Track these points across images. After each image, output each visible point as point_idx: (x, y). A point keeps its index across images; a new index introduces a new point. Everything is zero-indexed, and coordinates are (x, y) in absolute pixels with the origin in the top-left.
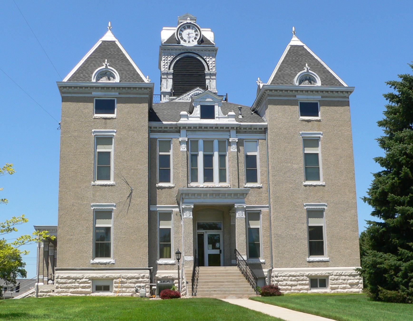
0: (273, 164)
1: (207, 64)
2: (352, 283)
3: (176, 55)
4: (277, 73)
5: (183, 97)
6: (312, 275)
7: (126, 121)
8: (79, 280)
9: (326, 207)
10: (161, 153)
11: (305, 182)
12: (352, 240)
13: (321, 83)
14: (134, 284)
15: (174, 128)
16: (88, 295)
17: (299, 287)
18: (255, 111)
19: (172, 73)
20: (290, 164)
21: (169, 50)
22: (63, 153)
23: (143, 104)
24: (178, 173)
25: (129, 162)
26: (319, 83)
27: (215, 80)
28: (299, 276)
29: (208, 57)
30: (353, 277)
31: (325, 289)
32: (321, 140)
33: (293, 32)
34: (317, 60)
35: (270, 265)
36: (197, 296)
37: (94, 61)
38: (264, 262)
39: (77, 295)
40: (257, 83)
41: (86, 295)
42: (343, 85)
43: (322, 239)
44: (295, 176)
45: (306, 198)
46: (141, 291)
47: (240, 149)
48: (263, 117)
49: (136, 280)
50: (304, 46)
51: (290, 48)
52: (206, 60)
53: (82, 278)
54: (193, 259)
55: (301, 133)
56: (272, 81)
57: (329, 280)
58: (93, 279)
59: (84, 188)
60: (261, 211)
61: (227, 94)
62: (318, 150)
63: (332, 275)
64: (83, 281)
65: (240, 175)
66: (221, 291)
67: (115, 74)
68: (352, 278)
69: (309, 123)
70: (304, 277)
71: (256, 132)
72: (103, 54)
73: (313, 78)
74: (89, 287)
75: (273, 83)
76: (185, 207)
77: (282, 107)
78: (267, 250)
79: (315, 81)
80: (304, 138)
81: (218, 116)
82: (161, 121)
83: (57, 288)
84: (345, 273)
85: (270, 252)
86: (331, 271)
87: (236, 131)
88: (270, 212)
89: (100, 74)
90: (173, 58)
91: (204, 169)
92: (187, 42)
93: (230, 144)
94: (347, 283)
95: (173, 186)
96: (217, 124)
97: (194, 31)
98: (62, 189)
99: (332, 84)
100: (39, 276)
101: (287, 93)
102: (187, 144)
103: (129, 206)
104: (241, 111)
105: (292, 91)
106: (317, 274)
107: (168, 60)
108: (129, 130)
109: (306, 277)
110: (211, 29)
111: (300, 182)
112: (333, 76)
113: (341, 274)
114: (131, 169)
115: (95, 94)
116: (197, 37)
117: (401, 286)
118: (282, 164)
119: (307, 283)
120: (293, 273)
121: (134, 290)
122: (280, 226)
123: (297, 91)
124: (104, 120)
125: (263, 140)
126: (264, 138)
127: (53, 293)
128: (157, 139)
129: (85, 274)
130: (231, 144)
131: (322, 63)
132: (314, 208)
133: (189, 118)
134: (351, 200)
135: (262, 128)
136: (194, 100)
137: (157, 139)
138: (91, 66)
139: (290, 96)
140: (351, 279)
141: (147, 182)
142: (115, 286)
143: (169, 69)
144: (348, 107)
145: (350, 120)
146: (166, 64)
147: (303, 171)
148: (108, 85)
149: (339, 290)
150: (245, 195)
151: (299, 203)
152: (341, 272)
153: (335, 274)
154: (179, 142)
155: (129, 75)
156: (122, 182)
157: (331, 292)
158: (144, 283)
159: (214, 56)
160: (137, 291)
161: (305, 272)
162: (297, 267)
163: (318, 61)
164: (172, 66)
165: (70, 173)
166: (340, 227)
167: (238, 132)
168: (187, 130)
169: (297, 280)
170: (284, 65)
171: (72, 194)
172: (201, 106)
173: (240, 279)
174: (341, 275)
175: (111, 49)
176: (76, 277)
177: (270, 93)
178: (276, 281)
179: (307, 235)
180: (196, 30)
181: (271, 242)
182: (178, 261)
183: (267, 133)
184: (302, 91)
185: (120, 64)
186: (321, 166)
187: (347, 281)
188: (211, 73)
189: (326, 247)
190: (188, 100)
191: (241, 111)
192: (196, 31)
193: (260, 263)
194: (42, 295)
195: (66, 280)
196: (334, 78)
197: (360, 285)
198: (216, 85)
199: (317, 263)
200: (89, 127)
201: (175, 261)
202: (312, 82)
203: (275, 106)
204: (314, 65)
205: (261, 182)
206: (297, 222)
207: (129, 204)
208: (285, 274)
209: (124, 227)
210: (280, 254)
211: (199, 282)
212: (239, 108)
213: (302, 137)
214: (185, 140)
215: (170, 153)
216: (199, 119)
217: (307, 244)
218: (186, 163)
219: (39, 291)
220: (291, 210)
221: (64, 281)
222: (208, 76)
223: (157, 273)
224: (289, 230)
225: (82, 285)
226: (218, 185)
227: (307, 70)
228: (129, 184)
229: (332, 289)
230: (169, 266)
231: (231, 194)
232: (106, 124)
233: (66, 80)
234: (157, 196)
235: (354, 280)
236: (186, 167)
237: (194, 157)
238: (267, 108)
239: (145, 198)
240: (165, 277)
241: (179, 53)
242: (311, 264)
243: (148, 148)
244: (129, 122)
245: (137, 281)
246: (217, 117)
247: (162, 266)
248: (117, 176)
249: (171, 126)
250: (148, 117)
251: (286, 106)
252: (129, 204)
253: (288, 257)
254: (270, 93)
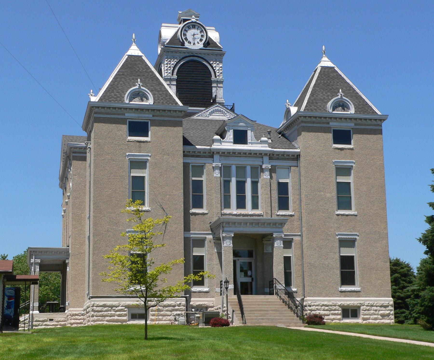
0: (306, 192)
1: (214, 70)
2: (383, 314)
3: (179, 59)
4: (309, 98)
5: (202, 114)
6: (345, 305)
7: (161, 145)
8: (114, 308)
9: (358, 237)
10: (194, 179)
11: (337, 211)
12: (383, 271)
13: (355, 110)
14: (170, 312)
15: (207, 153)
16: (124, 323)
17: (332, 317)
18: (282, 133)
19: (175, 79)
20: (323, 192)
21: (172, 53)
22: (97, 176)
23: (177, 127)
24: (211, 199)
25: (164, 187)
26: (352, 111)
27: (222, 88)
28: (331, 306)
29: (215, 62)
30: (384, 308)
31: (356, 319)
32: (353, 169)
33: (323, 52)
34: (348, 84)
35: (302, 294)
36: (247, 324)
37: (123, 78)
38: (296, 291)
39: (114, 323)
40: (286, 105)
41: (122, 324)
42: (376, 112)
43: (353, 269)
45: (339, 228)
46: (180, 319)
47: (273, 176)
48: (293, 141)
49: (173, 308)
50: (335, 67)
51: (321, 69)
52: (212, 65)
53: (118, 306)
54: (233, 287)
55: (334, 162)
56: (306, 106)
57: (361, 310)
58: (128, 307)
59: (119, 213)
60: (293, 239)
62: (350, 179)
63: (364, 305)
64: (119, 309)
65: (272, 203)
66: (269, 319)
67: (148, 95)
68: (383, 308)
69: (342, 151)
70: (337, 307)
71: (288, 159)
72: (132, 71)
73: (347, 105)
74: (125, 315)
75: (306, 109)
76: (225, 235)
77: (316, 134)
78: (299, 278)
79: (348, 108)
80: (337, 167)
81: (251, 142)
82: (192, 145)
83: (93, 316)
84: (377, 303)
85: (302, 281)
86: (363, 301)
87: (269, 157)
88: (302, 241)
89: (133, 94)
90: (177, 61)
91: (237, 196)
92: (192, 44)
93: (262, 170)
94: (378, 313)
95: (206, 212)
96: (250, 150)
97: (199, 31)
98: (96, 214)
99: (365, 112)
100: (34, 303)
101: (321, 120)
102: (220, 170)
103: (165, 232)
104: (270, 135)
105: (326, 118)
106: (349, 304)
107: (171, 64)
108: (164, 154)
109: (338, 307)
110: (215, 28)
111: (333, 211)
112: (365, 102)
113: (373, 305)
114: (167, 195)
115: (129, 115)
116: (202, 39)
117: (403, 319)
118: (315, 193)
119: (339, 313)
120: (325, 303)
121: (172, 318)
122: (313, 255)
123: (331, 118)
124: (138, 143)
125: (296, 168)
126: (296, 165)
127: (49, 322)
128: (190, 163)
129: (121, 302)
130: (264, 171)
131: (354, 87)
132: (346, 238)
133: (222, 143)
134: (382, 230)
135: (294, 155)
136: (227, 124)
137: (190, 163)
138: (121, 84)
139: (324, 123)
140: (382, 310)
141: (182, 208)
142: (152, 314)
143: (172, 75)
144: (381, 135)
145: (383, 149)
146: (169, 69)
147: (336, 200)
148: (143, 107)
149: (371, 321)
150: (283, 224)
151: (331, 232)
152: (372, 303)
153: (367, 304)
154: (212, 168)
155: (161, 96)
156: (157, 208)
157: (363, 322)
158: (180, 311)
159: (221, 62)
160: (175, 320)
161: (337, 302)
162: (329, 297)
163: (350, 85)
164: (175, 70)
165: (105, 197)
166: (371, 257)
167: (270, 159)
168: (220, 156)
169: (329, 310)
170: (316, 88)
171: (106, 219)
172: (234, 130)
173: (283, 308)
174: (372, 306)
175: (139, 66)
176: (112, 304)
177: (304, 119)
178: (309, 310)
179: (339, 265)
180: (201, 30)
181: (304, 271)
182: (227, 290)
183: (300, 160)
184: (336, 118)
185: (150, 83)
186: (353, 195)
187: (378, 312)
188: (218, 80)
189: (358, 277)
190: (207, 117)
191: (270, 135)
192: (201, 31)
193: (292, 292)
194: (37, 325)
195: (102, 308)
196: (367, 104)
197: (391, 317)
198: (223, 94)
199: (349, 293)
200: (123, 150)
201: (209, 289)
202: (345, 108)
203: (309, 133)
204: (346, 90)
205: (293, 210)
206: (329, 251)
207: (165, 231)
208: (318, 304)
209: (160, 254)
210: (312, 283)
211: (245, 310)
212: (268, 132)
213: (335, 166)
214: (219, 166)
215: (203, 178)
216: (232, 144)
217: (339, 274)
218: (220, 190)
219: (34, 321)
220: (323, 239)
221: (100, 309)
222: (214, 83)
223: (191, 301)
224: (321, 259)
225: (118, 313)
226: (251, 212)
227: (341, 96)
228: (164, 209)
229: (364, 319)
230: (203, 293)
231: (270, 224)
232: (140, 147)
234: (190, 222)
235: (386, 311)
236: (220, 194)
237: (227, 184)
238: (299, 134)
239: (180, 225)
240: (199, 305)
241: (183, 57)
242: (343, 293)
243: (183, 173)
244: (163, 146)
245: (173, 309)
246: (249, 143)
247: (196, 294)
248: (152, 202)
249: (205, 151)
250: (182, 142)
251: (319, 134)
252: (165, 231)
253: (320, 286)
254: (304, 119)
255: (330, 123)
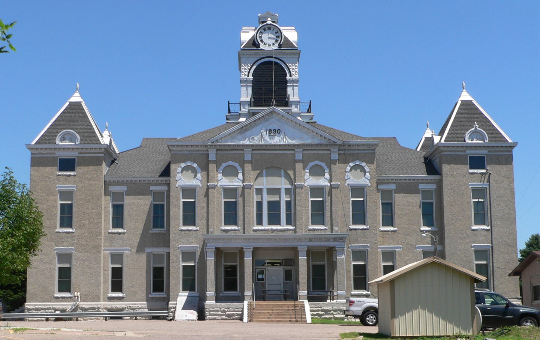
41: (478, 200)
44: (457, 171)
61: (310, 101)
188: (294, 79)
233: (33, 143)
255: (467, 151)
